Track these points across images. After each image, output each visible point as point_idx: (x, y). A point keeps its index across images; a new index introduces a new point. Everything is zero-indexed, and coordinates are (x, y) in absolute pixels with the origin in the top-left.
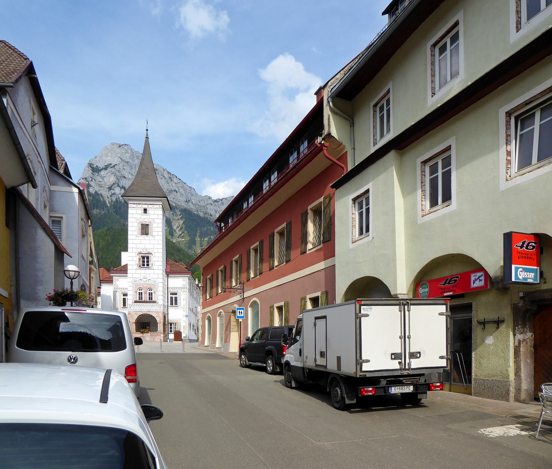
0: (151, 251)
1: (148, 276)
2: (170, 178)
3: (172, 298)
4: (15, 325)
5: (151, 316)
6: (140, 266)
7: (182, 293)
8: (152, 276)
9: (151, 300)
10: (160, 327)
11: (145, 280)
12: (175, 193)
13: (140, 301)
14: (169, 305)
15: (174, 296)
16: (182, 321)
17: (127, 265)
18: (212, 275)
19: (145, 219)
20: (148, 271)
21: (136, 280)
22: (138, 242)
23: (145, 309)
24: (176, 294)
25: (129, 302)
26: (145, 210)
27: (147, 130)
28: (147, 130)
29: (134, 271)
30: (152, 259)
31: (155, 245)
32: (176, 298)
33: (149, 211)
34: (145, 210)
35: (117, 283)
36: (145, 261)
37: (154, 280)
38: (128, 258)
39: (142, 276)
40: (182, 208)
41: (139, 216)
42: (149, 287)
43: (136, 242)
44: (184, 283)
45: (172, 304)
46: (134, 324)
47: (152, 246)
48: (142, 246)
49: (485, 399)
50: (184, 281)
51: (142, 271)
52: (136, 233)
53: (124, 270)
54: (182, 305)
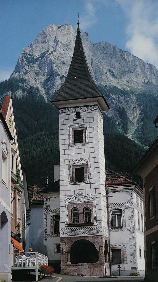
1: (83, 191)
2: (121, 56)
4: (9, 112)
5: (89, 242)
6: (73, 181)
7: (126, 210)
8: (89, 192)
9: (89, 223)
10: (102, 256)
11: (80, 197)
12: (129, 74)
13: (75, 224)
16: (128, 247)
17: (59, 180)
18: (154, 187)
19: (78, 124)
20: (83, 186)
22: (71, 152)
23: (79, 233)
25: (62, 226)
26: (78, 115)
27: (78, 24)
28: (78, 24)
29: (67, 188)
30: (90, 172)
31: (94, 153)
33: (84, 115)
34: (78, 115)
35: (48, 203)
36: (80, 174)
38: (64, 173)
39: (77, 192)
40: (139, 91)
41: (72, 122)
43: (69, 154)
47: (87, 156)
48: (76, 157)
49: (26, 235)
50: (128, 194)
51: (77, 187)
52: (68, 142)
53: (55, 188)
54: (127, 226)
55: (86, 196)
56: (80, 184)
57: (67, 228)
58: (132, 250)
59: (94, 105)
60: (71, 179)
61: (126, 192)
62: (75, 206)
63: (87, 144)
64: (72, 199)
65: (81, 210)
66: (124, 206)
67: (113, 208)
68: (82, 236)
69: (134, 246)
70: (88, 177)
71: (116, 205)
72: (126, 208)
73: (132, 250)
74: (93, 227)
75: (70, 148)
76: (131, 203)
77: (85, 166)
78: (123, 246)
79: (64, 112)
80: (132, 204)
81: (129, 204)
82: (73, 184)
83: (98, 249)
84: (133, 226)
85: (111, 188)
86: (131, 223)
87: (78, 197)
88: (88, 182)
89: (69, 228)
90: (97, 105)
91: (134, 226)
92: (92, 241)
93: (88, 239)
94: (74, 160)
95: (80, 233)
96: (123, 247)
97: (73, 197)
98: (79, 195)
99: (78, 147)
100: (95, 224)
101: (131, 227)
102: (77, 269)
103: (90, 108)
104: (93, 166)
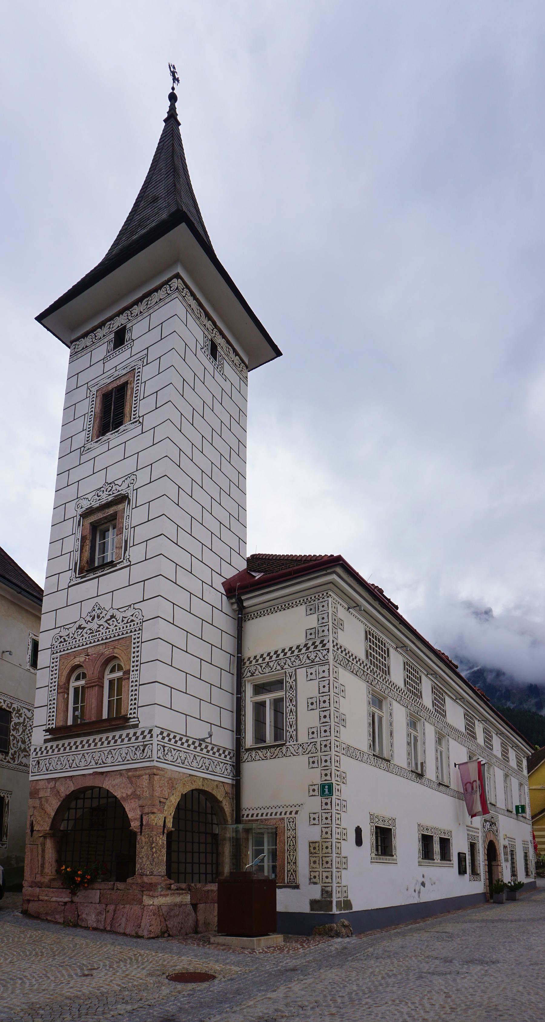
0: (123, 489)
1: (104, 602)
3: (259, 707)
5: (109, 795)
7: (301, 673)
14: (249, 740)
15: (268, 698)
16: (302, 821)
21: (64, 633)
23: (85, 760)
24: (278, 684)
27: (173, 98)
32: (278, 703)
37: (128, 614)
39: (87, 607)
42: (108, 652)
44: (313, 621)
45: (260, 737)
46: (49, 844)
48: (98, 481)
50: (311, 611)
51: (89, 588)
54: (303, 737)
55: (112, 617)
56: (98, 577)
57: (49, 745)
58: (317, 829)
59: (167, 282)
60: (76, 564)
61: (304, 607)
62: (77, 661)
63: (133, 426)
64: (71, 635)
65: (437, 857)
66: (293, 659)
67: (257, 673)
68: (91, 771)
69: (324, 758)
70: (126, 542)
71: (267, 659)
72: (301, 666)
73: (317, 829)
74: (124, 733)
75: (84, 458)
76: (322, 642)
77: (120, 507)
78: (283, 816)
79: (83, 349)
80: (324, 645)
81: (311, 649)
82: (79, 580)
83: (135, 825)
84: (323, 734)
85: (251, 601)
86: (316, 723)
87: (89, 626)
88: (126, 563)
89: (57, 743)
90: (177, 276)
91: (327, 704)
92: (118, 794)
93: (107, 784)
94: (89, 496)
95: (83, 763)
96: (283, 819)
97: (74, 629)
98: (93, 619)
99: (105, 447)
100: (132, 722)
101: (319, 740)
102: (65, 903)
103: (155, 297)
104: (143, 496)
